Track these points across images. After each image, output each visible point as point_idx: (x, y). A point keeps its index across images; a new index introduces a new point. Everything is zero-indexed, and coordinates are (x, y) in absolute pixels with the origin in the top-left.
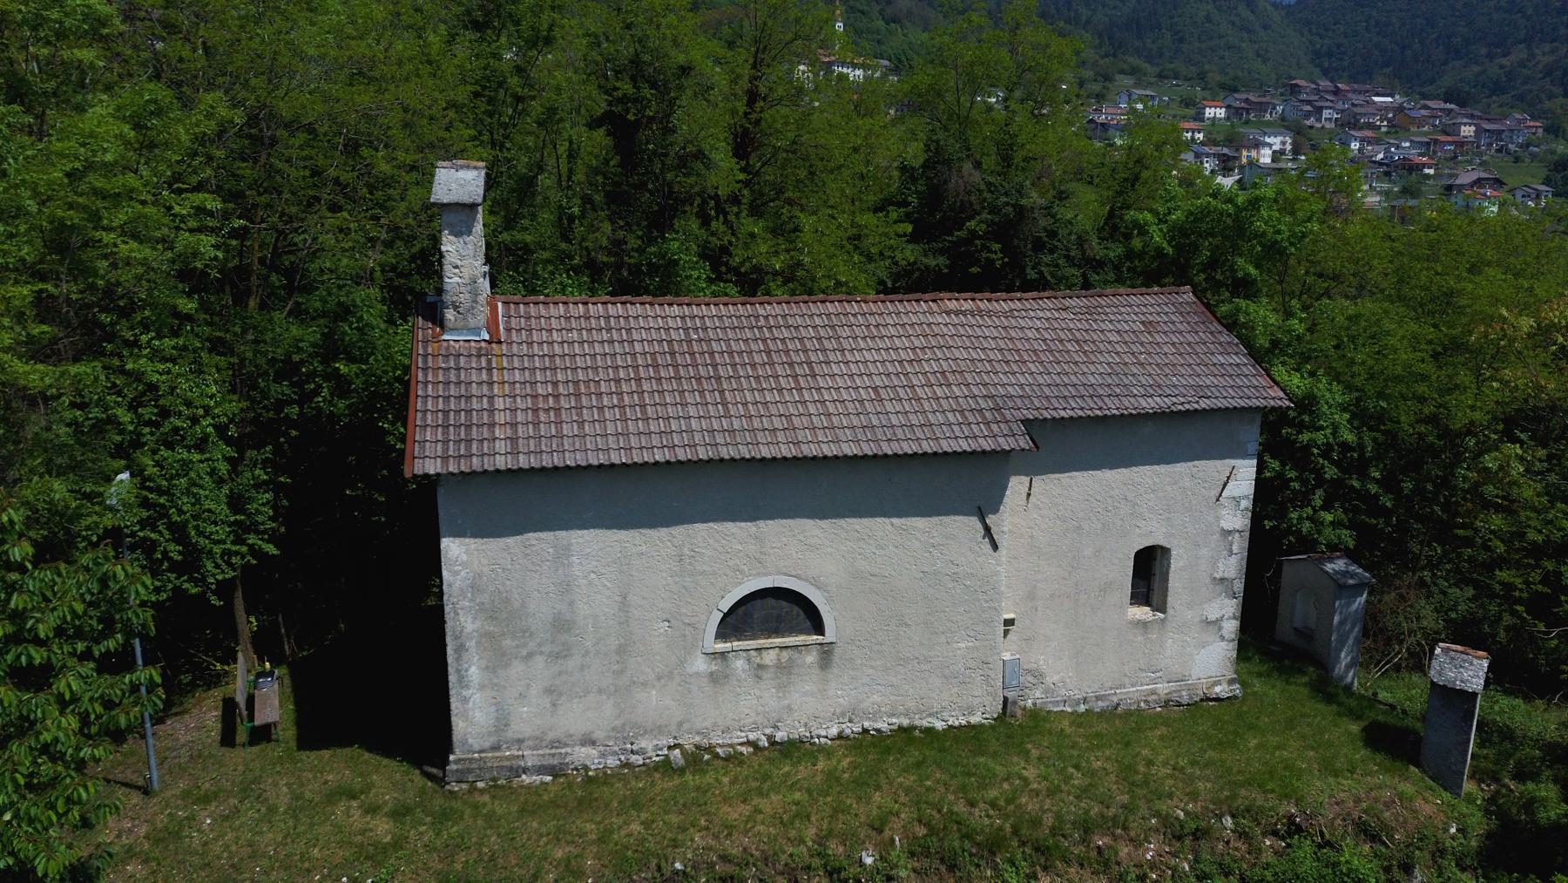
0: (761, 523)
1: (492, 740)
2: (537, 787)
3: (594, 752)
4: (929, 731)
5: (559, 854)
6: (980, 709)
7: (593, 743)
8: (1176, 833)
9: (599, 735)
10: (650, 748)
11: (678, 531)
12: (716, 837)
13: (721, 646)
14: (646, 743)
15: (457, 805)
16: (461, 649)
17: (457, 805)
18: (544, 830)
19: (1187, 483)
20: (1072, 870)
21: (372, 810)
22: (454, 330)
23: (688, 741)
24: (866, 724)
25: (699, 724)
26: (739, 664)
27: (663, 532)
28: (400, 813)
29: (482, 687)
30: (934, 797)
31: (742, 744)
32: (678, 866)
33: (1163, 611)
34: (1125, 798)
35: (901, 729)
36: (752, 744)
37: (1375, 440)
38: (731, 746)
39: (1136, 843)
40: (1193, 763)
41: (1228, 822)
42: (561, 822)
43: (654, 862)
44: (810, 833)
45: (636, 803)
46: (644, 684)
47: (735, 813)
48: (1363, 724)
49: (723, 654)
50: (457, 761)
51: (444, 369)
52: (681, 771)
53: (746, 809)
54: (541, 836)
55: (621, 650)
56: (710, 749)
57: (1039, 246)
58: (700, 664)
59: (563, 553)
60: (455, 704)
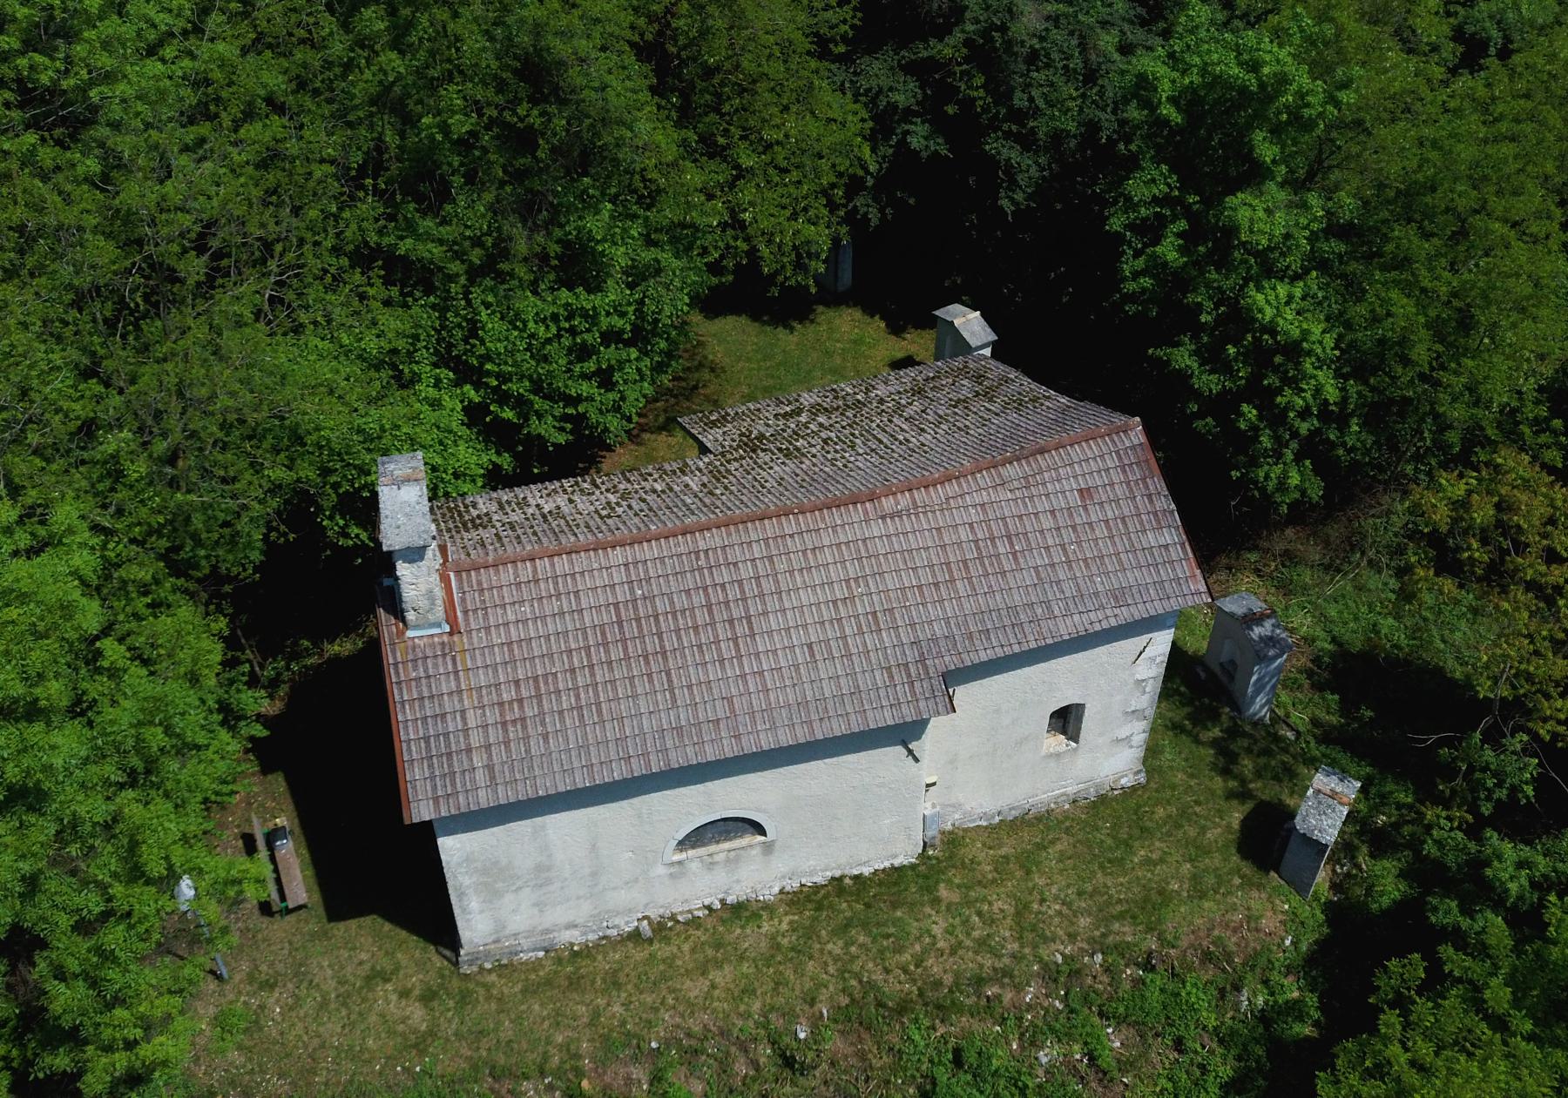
0: (709, 784)
1: (493, 937)
2: (533, 963)
3: (576, 933)
4: (857, 878)
5: (560, 1039)
6: (905, 853)
7: (576, 926)
8: (1050, 974)
9: (580, 921)
10: (623, 923)
11: (636, 801)
12: (682, 1016)
13: (678, 857)
15: (471, 986)
16: (461, 895)
18: (545, 1013)
19: (1105, 658)
20: (964, 1019)
21: (404, 994)
23: (654, 914)
24: (803, 881)
26: (694, 866)
27: (624, 803)
28: (428, 997)
29: (481, 912)
30: (856, 967)
31: (699, 909)
32: (654, 1045)
33: (1077, 741)
36: (709, 908)
37: (1359, 393)
38: (690, 911)
39: (1019, 989)
41: (1099, 958)
42: (558, 1004)
43: (635, 1042)
44: (757, 1006)
45: (614, 982)
46: (614, 889)
47: (694, 989)
48: (1249, 805)
49: (680, 863)
50: (466, 955)
51: (415, 679)
52: (650, 941)
54: (544, 1020)
55: (594, 874)
56: (673, 917)
58: (661, 870)
59: (543, 827)
60: (460, 923)
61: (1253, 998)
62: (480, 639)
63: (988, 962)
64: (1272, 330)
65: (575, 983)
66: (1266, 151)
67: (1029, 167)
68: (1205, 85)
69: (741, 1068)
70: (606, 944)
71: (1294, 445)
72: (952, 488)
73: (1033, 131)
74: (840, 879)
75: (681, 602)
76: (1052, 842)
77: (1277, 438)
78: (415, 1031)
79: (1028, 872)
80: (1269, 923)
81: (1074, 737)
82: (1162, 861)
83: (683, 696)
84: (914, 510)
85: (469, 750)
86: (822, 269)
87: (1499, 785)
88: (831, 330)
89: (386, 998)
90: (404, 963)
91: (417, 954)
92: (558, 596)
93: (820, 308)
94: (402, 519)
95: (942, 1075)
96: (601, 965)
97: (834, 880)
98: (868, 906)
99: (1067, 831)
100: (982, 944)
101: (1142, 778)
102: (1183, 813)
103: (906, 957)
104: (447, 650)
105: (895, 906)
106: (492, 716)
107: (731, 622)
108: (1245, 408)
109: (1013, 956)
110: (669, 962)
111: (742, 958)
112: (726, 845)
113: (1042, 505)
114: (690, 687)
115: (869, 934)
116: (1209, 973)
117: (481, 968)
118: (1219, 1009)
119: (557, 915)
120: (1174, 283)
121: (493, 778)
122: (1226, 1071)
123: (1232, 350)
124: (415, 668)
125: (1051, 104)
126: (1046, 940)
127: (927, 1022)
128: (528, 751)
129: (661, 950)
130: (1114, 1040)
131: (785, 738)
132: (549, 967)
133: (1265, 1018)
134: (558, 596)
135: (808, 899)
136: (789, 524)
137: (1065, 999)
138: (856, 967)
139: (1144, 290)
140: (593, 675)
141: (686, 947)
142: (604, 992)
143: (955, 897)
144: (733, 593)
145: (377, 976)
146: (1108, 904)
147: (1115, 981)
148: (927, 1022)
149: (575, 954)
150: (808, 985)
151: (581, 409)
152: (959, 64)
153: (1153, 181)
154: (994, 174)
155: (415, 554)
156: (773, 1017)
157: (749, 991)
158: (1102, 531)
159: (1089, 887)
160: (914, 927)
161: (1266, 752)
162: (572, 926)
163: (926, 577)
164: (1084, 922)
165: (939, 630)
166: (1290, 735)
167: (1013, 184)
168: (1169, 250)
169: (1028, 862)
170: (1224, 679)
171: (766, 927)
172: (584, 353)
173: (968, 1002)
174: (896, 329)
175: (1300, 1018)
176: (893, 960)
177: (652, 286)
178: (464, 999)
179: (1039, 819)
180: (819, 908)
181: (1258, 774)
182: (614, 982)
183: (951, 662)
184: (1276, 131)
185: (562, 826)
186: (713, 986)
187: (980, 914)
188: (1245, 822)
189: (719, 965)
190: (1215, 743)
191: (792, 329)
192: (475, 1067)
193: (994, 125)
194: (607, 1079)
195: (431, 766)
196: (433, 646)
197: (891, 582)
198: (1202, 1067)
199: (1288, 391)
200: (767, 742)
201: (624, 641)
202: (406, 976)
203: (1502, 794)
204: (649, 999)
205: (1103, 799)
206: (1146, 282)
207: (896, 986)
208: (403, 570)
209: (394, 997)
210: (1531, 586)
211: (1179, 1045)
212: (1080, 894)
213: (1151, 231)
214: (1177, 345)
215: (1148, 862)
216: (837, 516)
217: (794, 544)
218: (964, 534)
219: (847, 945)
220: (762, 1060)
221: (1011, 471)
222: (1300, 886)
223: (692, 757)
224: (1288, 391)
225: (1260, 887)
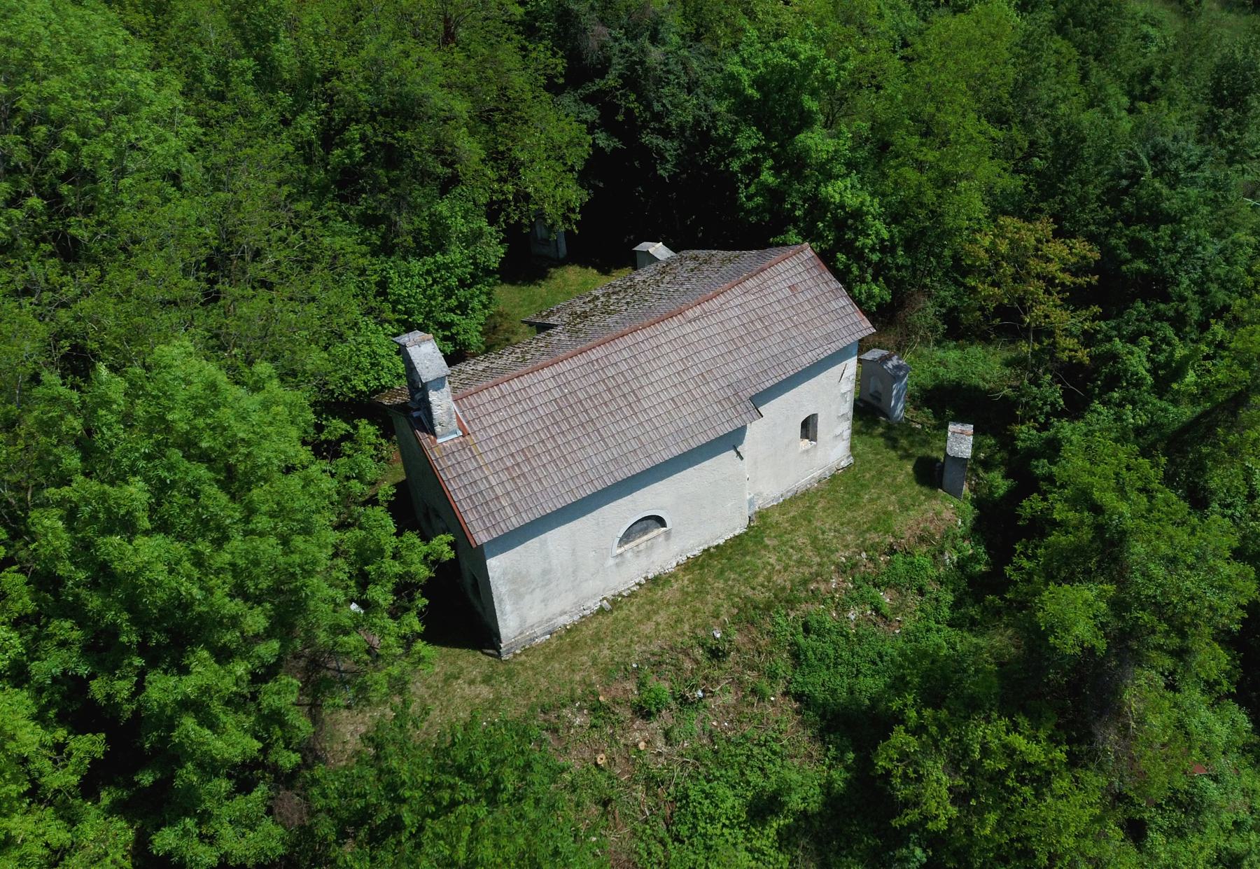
4: (717, 547)
5: (578, 678)
8: (841, 570)
9: (568, 608)
14: (590, 604)
15: (511, 666)
16: (501, 601)
17: (511, 666)
21: (472, 682)
22: (443, 436)
23: (609, 595)
25: (612, 586)
27: (589, 516)
28: (487, 680)
30: (735, 591)
34: (818, 559)
35: (704, 550)
36: (639, 584)
39: (827, 581)
40: (842, 524)
41: (864, 555)
44: (686, 627)
45: (598, 639)
47: (648, 628)
48: (913, 462)
49: (621, 554)
52: (611, 611)
53: (652, 624)
56: (620, 595)
57: (659, 82)
58: (611, 562)
61: (951, 557)
62: (481, 436)
63: (806, 571)
64: (842, 206)
65: (574, 646)
66: (810, 104)
67: (670, 147)
68: (768, 73)
69: (688, 665)
71: (870, 271)
72: (722, 299)
73: (668, 125)
75: (593, 391)
76: (816, 504)
77: (860, 268)
78: (487, 700)
79: (810, 521)
80: (947, 515)
81: (814, 439)
82: (879, 498)
83: (611, 442)
85: (497, 498)
86: (579, 217)
87: (1045, 404)
88: (565, 280)
89: (461, 687)
90: (464, 666)
91: (471, 659)
92: (520, 402)
93: (552, 270)
94: (428, 363)
95: (800, 639)
96: (587, 632)
97: (706, 551)
98: (729, 559)
99: (821, 496)
100: (800, 562)
101: (851, 460)
102: (880, 472)
103: (761, 579)
104: (464, 446)
105: (744, 555)
106: (504, 476)
107: (624, 395)
108: (839, 255)
109: (819, 565)
110: (626, 619)
111: (668, 604)
112: (645, 538)
113: (772, 299)
114: (613, 436)
115: (736, 572)
116: (924, 548)
117: (515, 655)
118: (935, 566)
119: (555, 607)
120: (775, 195)
121: (517, 509)
122: (950, 598)
123: (821, 225)
124: (449, 459)
125: (675, 106)
126: (832, 552)
127: (784, 612)
128: (532, 490)
130: (886, 598)
131: (676, 451)
132: (555, 643)
133: (961, 565)
134: (520, 402)
135: (694, 564)
136: (640, 336)
137: (853, 582)
138: (735, 591)
139: (758, 206)
140: (555, 441)
141: (633, 609)
142: (595, 645)
143: (776, 542)
144: (620, 380)
145: (449, 679)
146: (859, 525)
147: (876, 565)
148: (784, 612)
149: (569, 631)
150: (712, 608)
151: (454, 331)
152: (618, 90)
153: (750, 137)
154: (650, 157)
155: (439, 383)
156: (698, 631)
157: (679, 621)
158: (807, 307)
159: (845, 520)
160: (759, 563)
161: (910, 435)
162: (563, 613)
164: (849, 538)
165: (740, 376)
166: (919, 426)
167: (664, 160)
168: (767, 177)
170: (874, 402)
171: (675, 586)
172: (449, 293)
173: (803, 595)
174: (605, 270)
175: (978, 562)
176: (754, 583)
177: (480, 246)
178: (510, 675)
179: (804, 494)
180: (702, 567)
181: (912, 444)
182: (598, 639)
184: (814, 93)
185: (556, 538)
186: (658, 624)
187: (792, 547)
188: (915, 468)
189: (656, 613)
190: (882, 435)
191: (540, 285)
192: (532, 709)
193: (645, 125)
194: (613, 693)
195: (478, 512)
196: (455, 445)
198: (937, 600)
199: (861, 238)
200: (667, 456)
201: (567, 419)
202: (469, 673)
203: (1047, 408)
204: (622, 641)
205: (833, 476)
206: (759, 200)
207: (761, 596)
208: (433, 396)
209: (466, 686)
210: (1038, 277)
211: (921, 592)
212: (842, 524)
213: (752, 170)
214: (787, 232)
215: (871, 500)
216: (663, 326)
218: (736, 322)
219: (726, 581)
220: (699, 658)
221: (750, 283)
222: (956, 493)
223: (625, 473)
224: (861, 238)
225: (935, 498)
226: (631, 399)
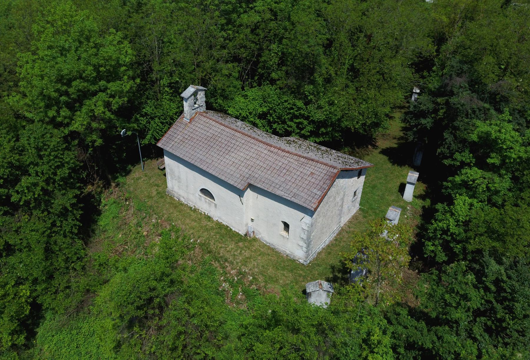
4: (231, 229)
6: (242, 232)
8: (240, 273)
41: (251, 278)
56: (198, 210)
65: (176, 207)
70: (186, 206)
74: (228, 227)
84: (276, 153)
103: (220, 245)
104: (186, 124)
110: (190, 215)
119: (223, 218)
129: (192, 213)
150: (202, 235)
163: (265, 166)
169: (262, 254)
179: (276, 252)
183: (252, 182)
187: (241, 251)
197: (258, 162)
207: (212, 247)
217: (249, 144)
226: (227, 152)
